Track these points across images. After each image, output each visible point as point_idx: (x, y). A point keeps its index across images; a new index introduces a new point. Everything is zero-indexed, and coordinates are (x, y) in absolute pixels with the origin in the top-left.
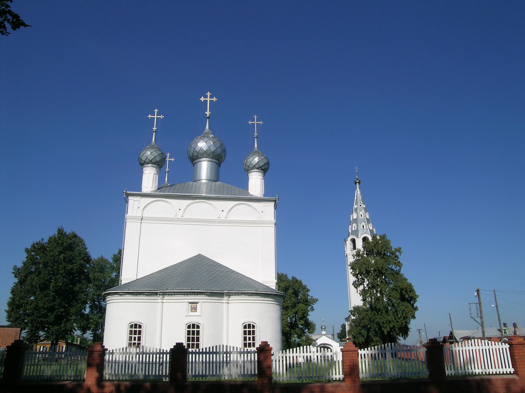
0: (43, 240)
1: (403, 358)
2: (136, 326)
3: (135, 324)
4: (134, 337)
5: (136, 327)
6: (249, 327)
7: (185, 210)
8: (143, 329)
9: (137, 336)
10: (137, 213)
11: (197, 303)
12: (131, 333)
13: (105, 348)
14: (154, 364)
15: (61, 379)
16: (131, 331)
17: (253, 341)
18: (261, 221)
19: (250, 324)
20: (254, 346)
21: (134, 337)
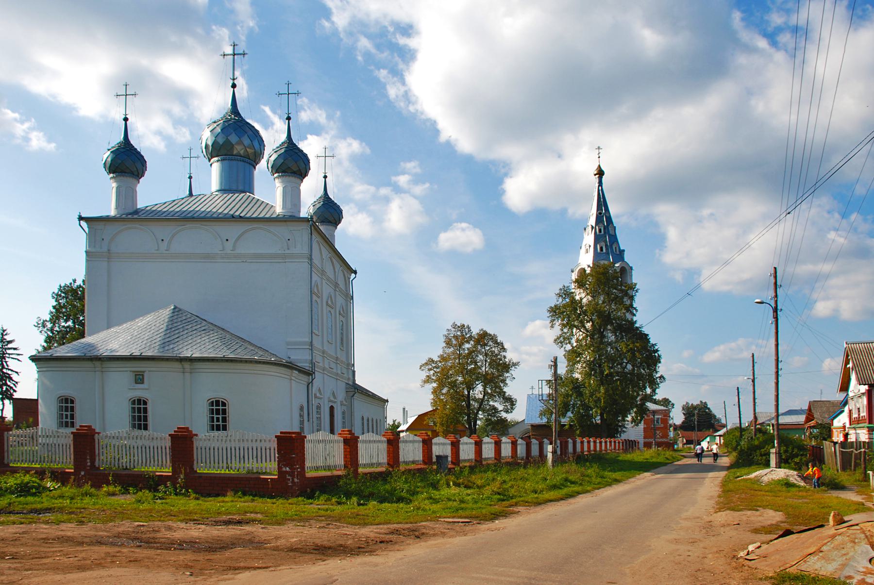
0: (75, 281)
1: (117, 437)
2: (217, 403)
3: (138, 399)
4: (217, 418)
5: (139, 403)
6: (67, 402)
7: (170, 242)
8: (77, 406)
9: (69, 413)
10: (101, 248)
11: (144, 372)
12: (61, 408)
13: (194, 433)
14: (435, 462)
15: (844, 516)
16: (133, 409)
17: (71, 419)
18: (240, 261)
19: (219, 401)
20: (73, 426)
21: (217, 418)
